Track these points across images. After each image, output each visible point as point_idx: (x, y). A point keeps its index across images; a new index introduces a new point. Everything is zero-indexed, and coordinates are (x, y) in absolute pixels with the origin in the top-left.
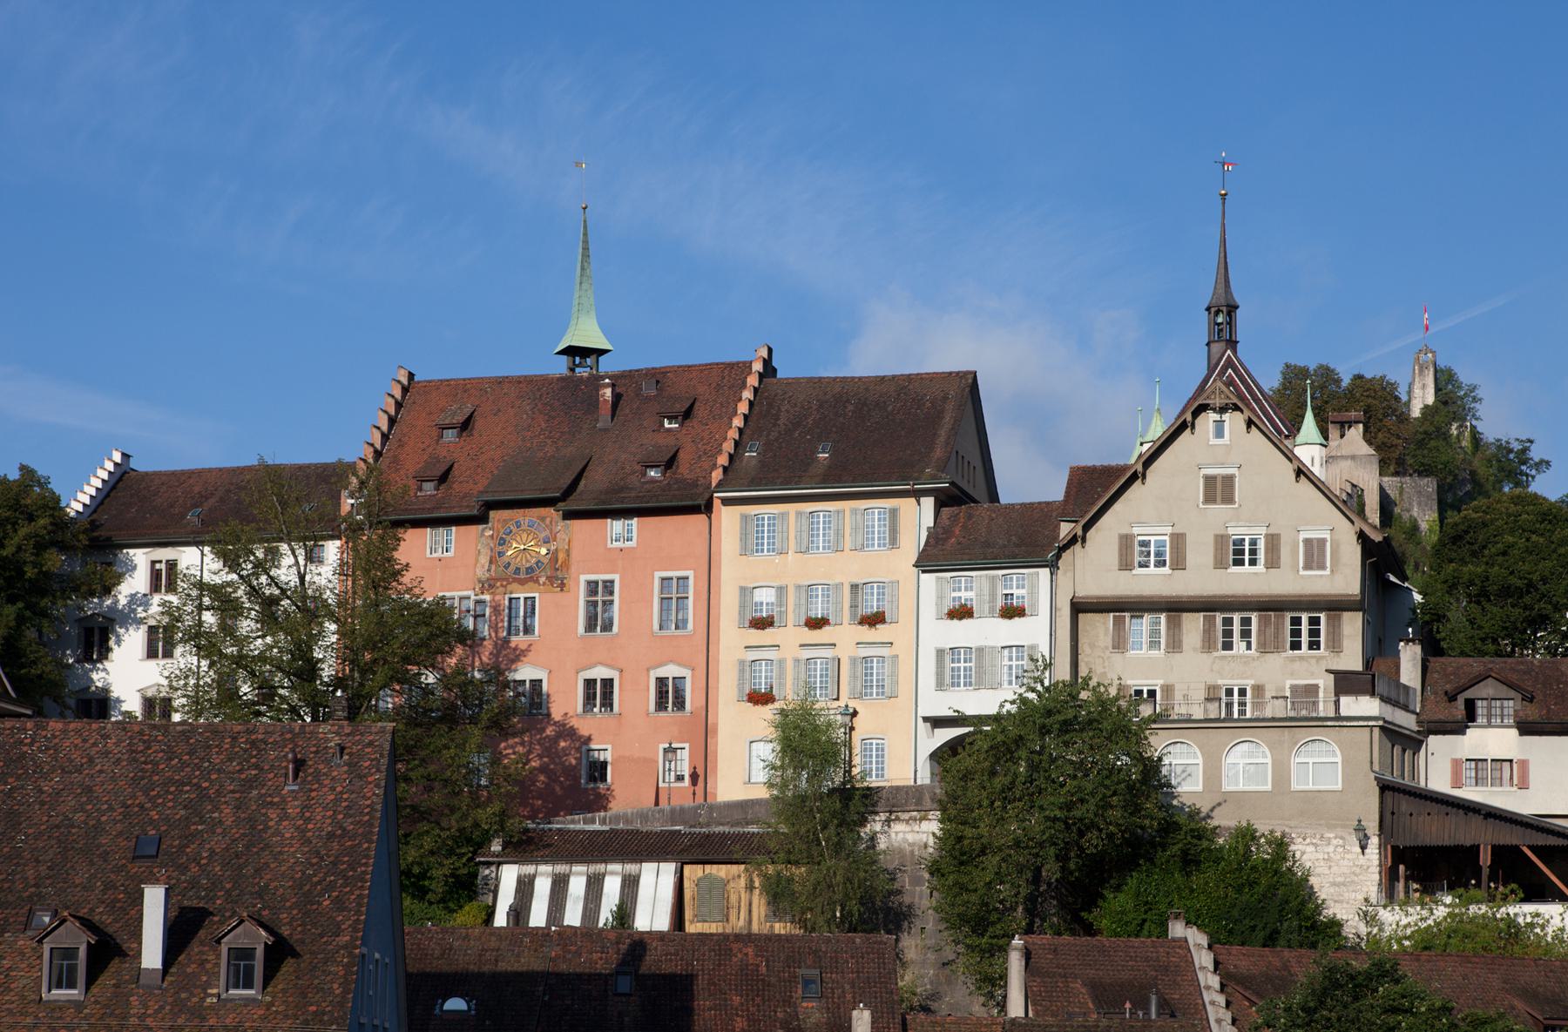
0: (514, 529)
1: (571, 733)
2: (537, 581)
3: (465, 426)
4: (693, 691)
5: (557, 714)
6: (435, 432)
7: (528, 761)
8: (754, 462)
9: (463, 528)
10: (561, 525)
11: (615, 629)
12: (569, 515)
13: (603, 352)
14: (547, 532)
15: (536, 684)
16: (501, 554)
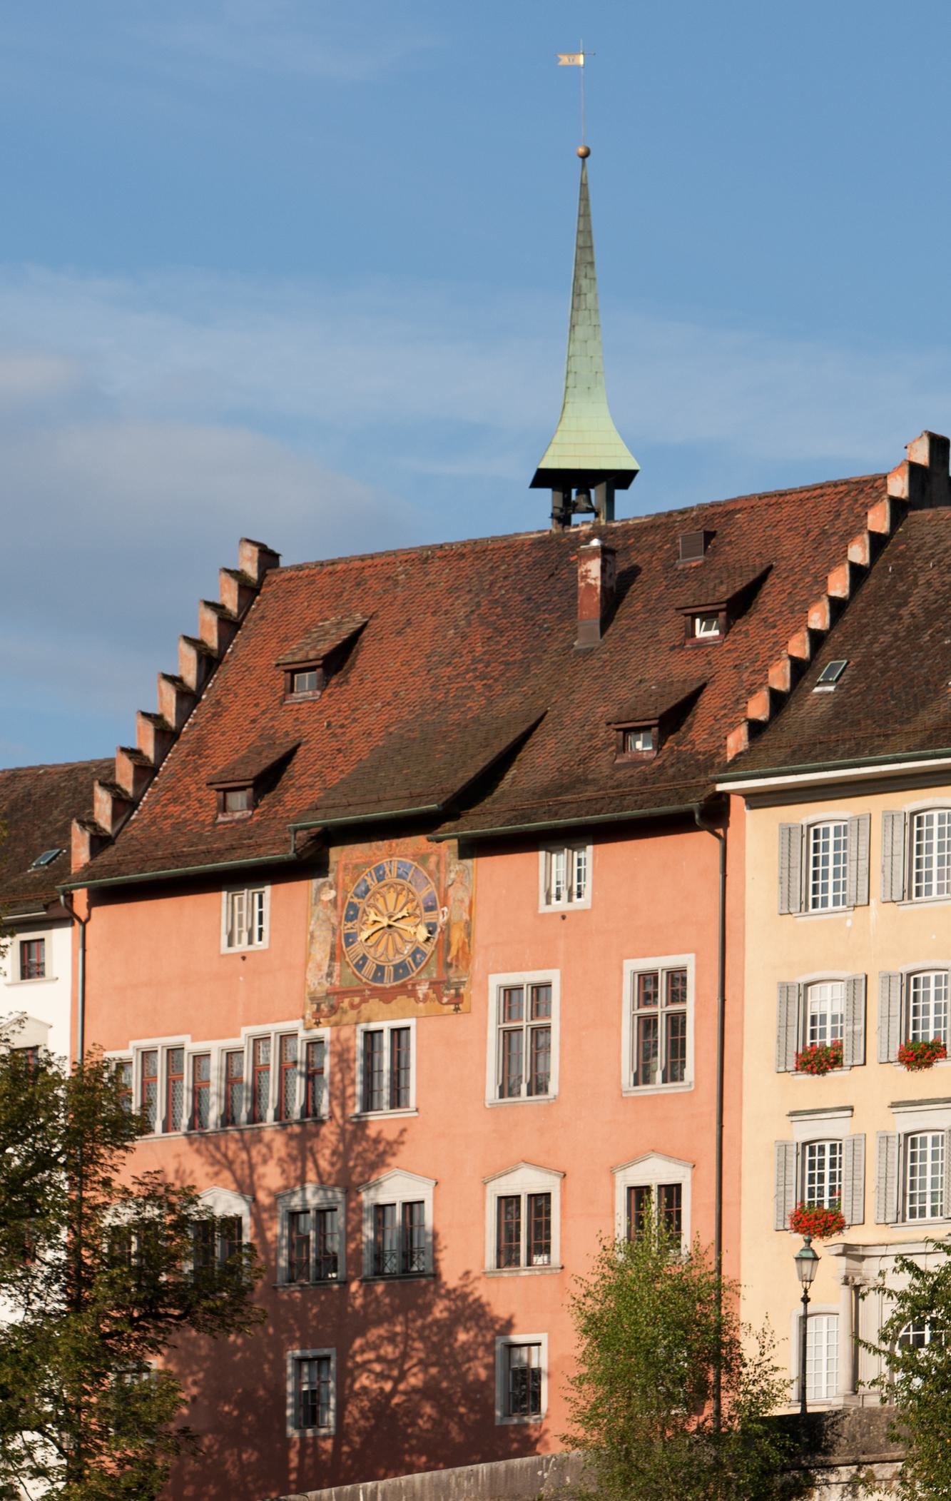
0: (372, 883)
1: (472, 1312)
2: (412, 994)
3: (336, 662)
4: (694, 1210)
5: (451, 1278)
6: (281, 680)
7: (403, 1376)
8: (824, 707)
9: (284, 888)
10: (457, 869)
11: (553, 1086)
12: (473, 848)
13: (623, 478)
14: (431, 888)
15: (411, 1208)
16: (350, 938)
